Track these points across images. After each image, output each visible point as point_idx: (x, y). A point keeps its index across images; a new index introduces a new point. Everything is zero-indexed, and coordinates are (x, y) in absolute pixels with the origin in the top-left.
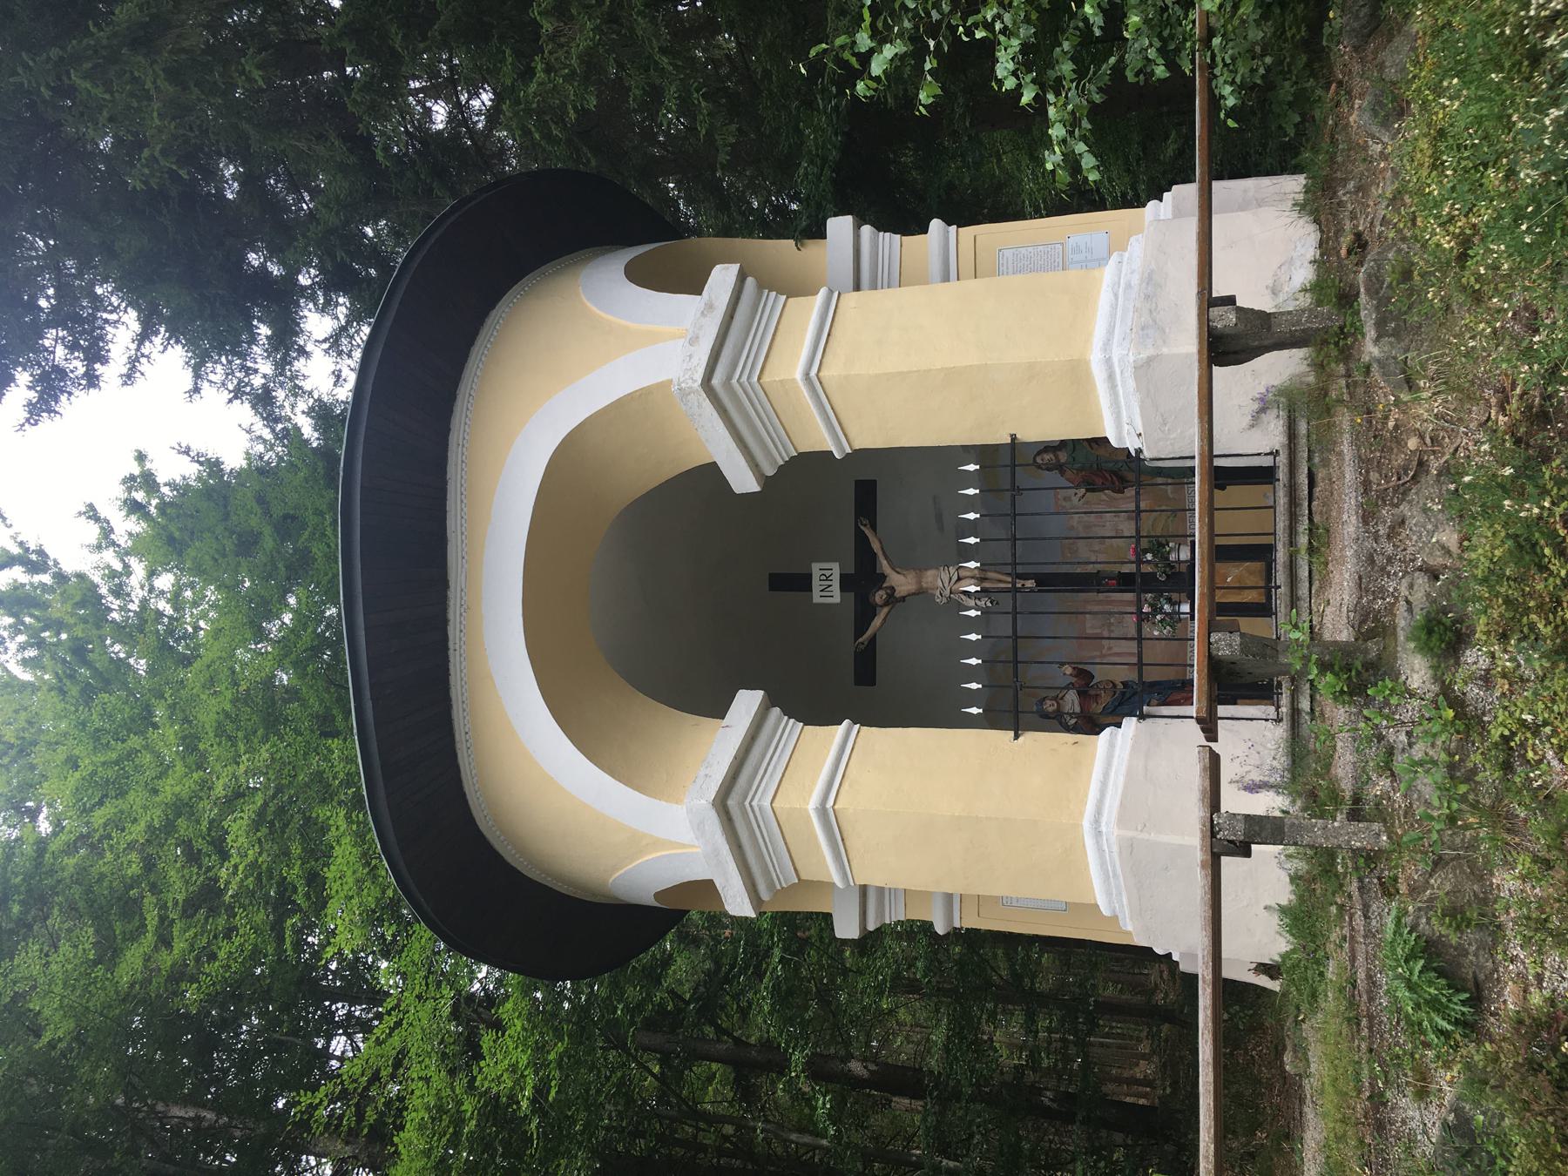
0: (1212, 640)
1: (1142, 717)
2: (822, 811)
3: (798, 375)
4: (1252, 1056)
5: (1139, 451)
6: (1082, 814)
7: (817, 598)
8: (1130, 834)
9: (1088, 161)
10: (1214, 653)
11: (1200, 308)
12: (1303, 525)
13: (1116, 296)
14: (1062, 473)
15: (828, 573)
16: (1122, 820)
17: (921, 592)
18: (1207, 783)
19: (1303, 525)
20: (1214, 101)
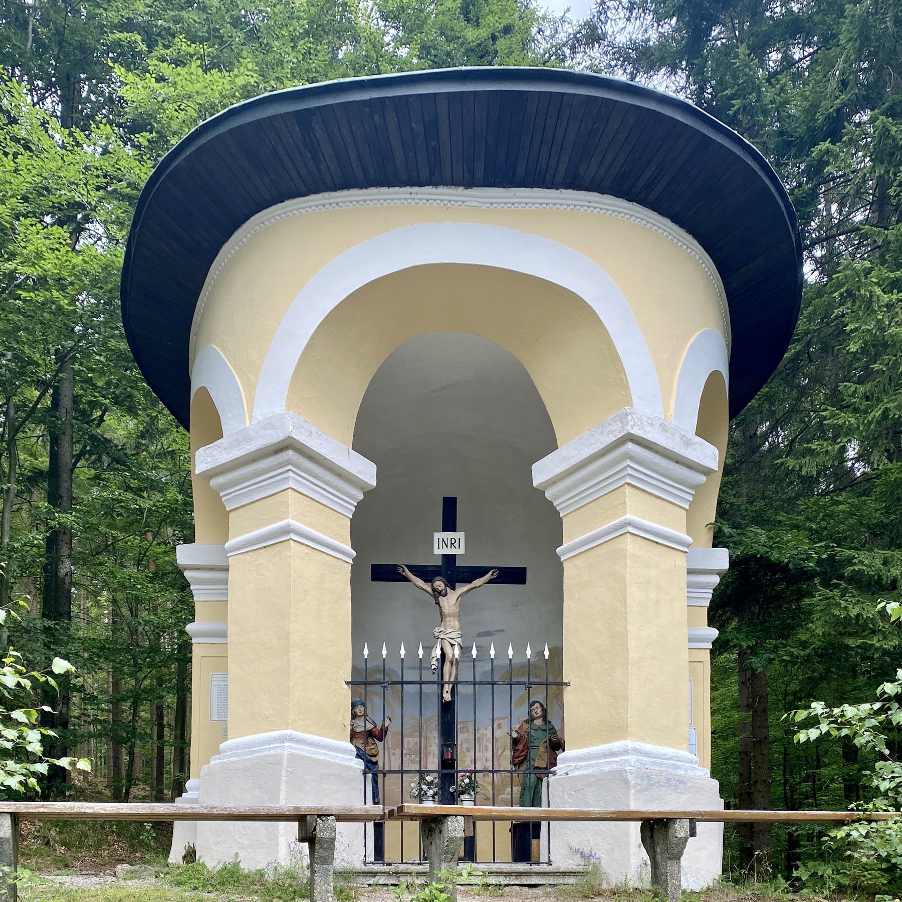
0: (459, 818)
1: (365, 773)
2: (287, 530)
3: (629, 516)
4: (114, 845)
5: (554, 773)
6: (295, 729)
7: (439, 536)
8: (285, 763)
9: (813, 734)
10: (450, 819)
11: (690, 813)
12: (503, 881)
13: (670, 759)
14: (527, 721)
15: (456, 545)
16: (292, 756)
17: (442, 616)
18: (357, 812)
19: (503, 881)
20: (840, 823)
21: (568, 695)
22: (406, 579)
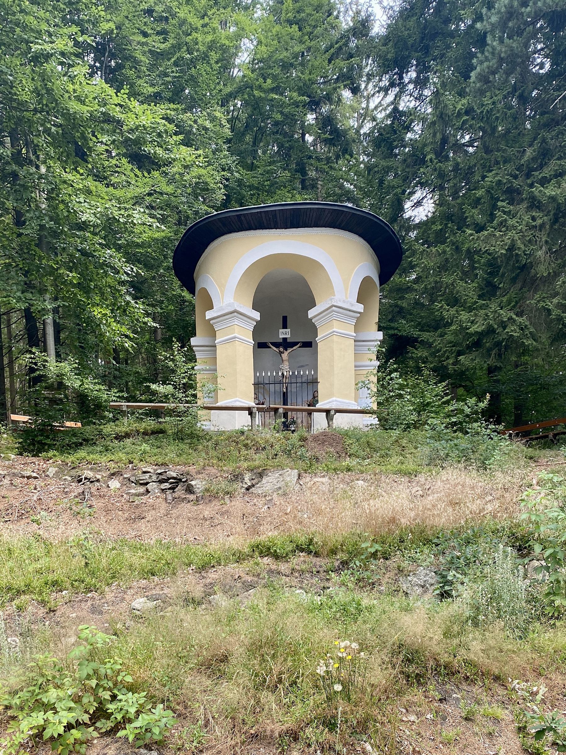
2: (235, 338)
3: (335, 329)
7: (281, 330)
21: (320, 386)
22: (270, 347)
